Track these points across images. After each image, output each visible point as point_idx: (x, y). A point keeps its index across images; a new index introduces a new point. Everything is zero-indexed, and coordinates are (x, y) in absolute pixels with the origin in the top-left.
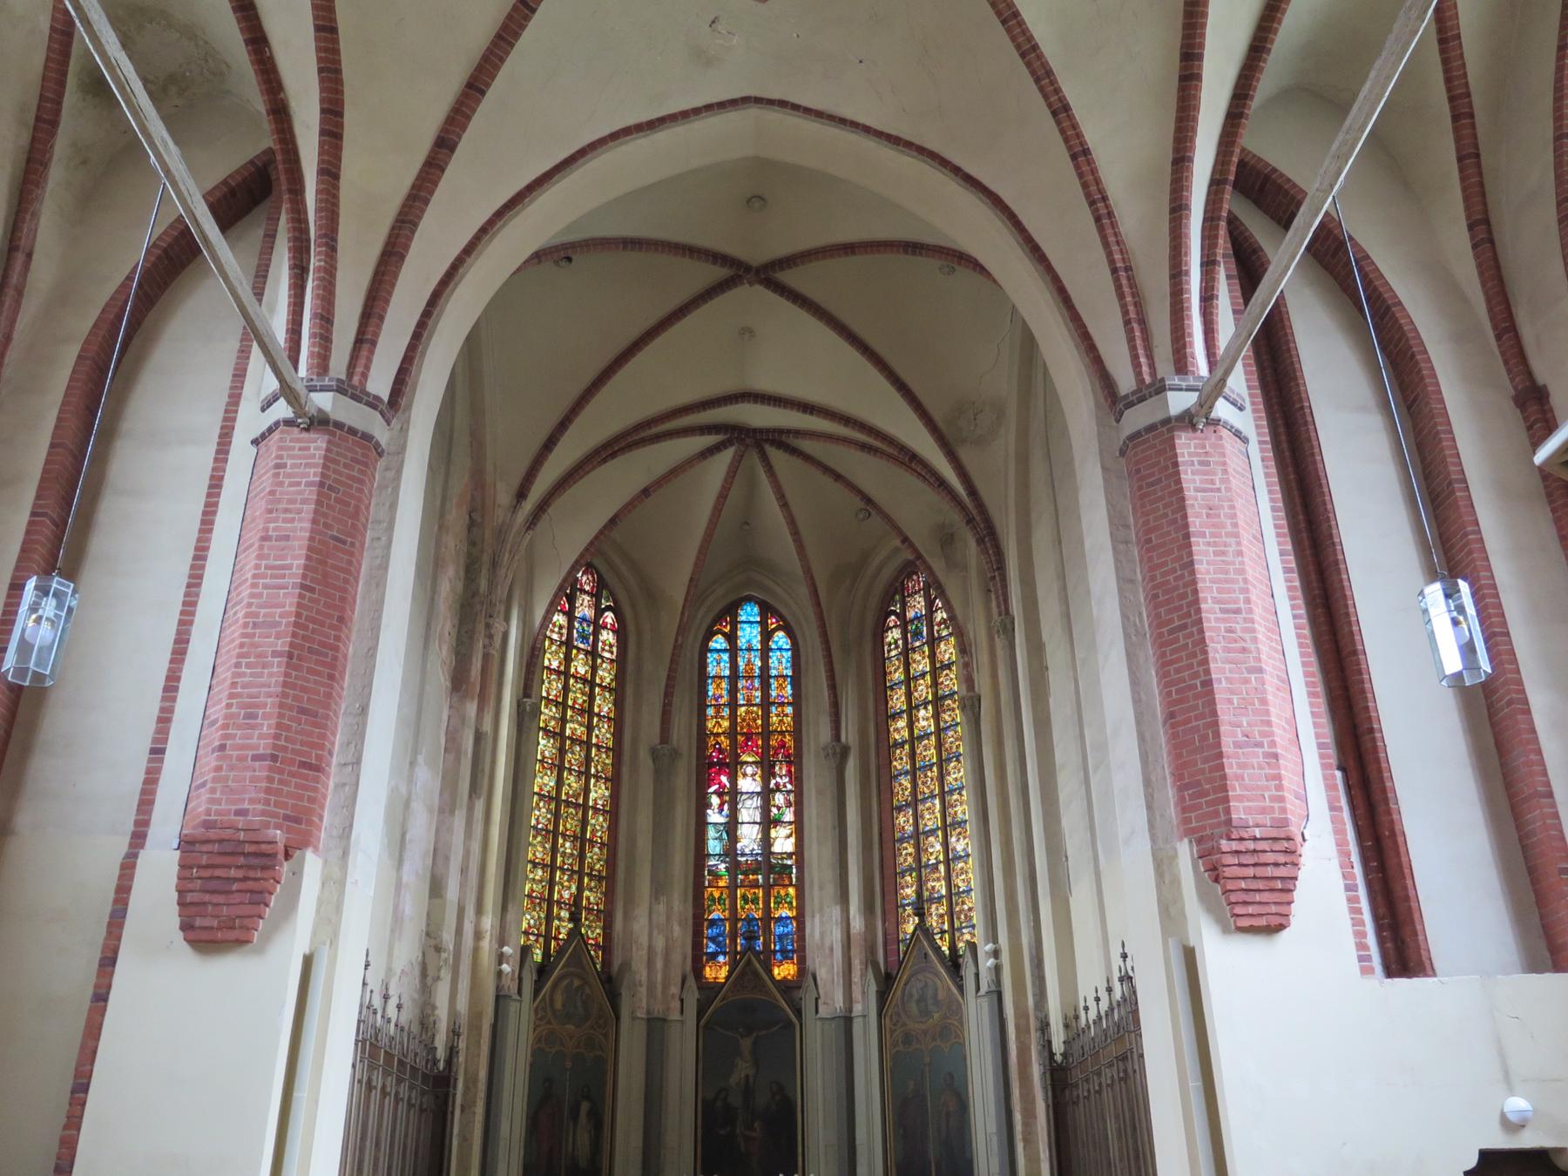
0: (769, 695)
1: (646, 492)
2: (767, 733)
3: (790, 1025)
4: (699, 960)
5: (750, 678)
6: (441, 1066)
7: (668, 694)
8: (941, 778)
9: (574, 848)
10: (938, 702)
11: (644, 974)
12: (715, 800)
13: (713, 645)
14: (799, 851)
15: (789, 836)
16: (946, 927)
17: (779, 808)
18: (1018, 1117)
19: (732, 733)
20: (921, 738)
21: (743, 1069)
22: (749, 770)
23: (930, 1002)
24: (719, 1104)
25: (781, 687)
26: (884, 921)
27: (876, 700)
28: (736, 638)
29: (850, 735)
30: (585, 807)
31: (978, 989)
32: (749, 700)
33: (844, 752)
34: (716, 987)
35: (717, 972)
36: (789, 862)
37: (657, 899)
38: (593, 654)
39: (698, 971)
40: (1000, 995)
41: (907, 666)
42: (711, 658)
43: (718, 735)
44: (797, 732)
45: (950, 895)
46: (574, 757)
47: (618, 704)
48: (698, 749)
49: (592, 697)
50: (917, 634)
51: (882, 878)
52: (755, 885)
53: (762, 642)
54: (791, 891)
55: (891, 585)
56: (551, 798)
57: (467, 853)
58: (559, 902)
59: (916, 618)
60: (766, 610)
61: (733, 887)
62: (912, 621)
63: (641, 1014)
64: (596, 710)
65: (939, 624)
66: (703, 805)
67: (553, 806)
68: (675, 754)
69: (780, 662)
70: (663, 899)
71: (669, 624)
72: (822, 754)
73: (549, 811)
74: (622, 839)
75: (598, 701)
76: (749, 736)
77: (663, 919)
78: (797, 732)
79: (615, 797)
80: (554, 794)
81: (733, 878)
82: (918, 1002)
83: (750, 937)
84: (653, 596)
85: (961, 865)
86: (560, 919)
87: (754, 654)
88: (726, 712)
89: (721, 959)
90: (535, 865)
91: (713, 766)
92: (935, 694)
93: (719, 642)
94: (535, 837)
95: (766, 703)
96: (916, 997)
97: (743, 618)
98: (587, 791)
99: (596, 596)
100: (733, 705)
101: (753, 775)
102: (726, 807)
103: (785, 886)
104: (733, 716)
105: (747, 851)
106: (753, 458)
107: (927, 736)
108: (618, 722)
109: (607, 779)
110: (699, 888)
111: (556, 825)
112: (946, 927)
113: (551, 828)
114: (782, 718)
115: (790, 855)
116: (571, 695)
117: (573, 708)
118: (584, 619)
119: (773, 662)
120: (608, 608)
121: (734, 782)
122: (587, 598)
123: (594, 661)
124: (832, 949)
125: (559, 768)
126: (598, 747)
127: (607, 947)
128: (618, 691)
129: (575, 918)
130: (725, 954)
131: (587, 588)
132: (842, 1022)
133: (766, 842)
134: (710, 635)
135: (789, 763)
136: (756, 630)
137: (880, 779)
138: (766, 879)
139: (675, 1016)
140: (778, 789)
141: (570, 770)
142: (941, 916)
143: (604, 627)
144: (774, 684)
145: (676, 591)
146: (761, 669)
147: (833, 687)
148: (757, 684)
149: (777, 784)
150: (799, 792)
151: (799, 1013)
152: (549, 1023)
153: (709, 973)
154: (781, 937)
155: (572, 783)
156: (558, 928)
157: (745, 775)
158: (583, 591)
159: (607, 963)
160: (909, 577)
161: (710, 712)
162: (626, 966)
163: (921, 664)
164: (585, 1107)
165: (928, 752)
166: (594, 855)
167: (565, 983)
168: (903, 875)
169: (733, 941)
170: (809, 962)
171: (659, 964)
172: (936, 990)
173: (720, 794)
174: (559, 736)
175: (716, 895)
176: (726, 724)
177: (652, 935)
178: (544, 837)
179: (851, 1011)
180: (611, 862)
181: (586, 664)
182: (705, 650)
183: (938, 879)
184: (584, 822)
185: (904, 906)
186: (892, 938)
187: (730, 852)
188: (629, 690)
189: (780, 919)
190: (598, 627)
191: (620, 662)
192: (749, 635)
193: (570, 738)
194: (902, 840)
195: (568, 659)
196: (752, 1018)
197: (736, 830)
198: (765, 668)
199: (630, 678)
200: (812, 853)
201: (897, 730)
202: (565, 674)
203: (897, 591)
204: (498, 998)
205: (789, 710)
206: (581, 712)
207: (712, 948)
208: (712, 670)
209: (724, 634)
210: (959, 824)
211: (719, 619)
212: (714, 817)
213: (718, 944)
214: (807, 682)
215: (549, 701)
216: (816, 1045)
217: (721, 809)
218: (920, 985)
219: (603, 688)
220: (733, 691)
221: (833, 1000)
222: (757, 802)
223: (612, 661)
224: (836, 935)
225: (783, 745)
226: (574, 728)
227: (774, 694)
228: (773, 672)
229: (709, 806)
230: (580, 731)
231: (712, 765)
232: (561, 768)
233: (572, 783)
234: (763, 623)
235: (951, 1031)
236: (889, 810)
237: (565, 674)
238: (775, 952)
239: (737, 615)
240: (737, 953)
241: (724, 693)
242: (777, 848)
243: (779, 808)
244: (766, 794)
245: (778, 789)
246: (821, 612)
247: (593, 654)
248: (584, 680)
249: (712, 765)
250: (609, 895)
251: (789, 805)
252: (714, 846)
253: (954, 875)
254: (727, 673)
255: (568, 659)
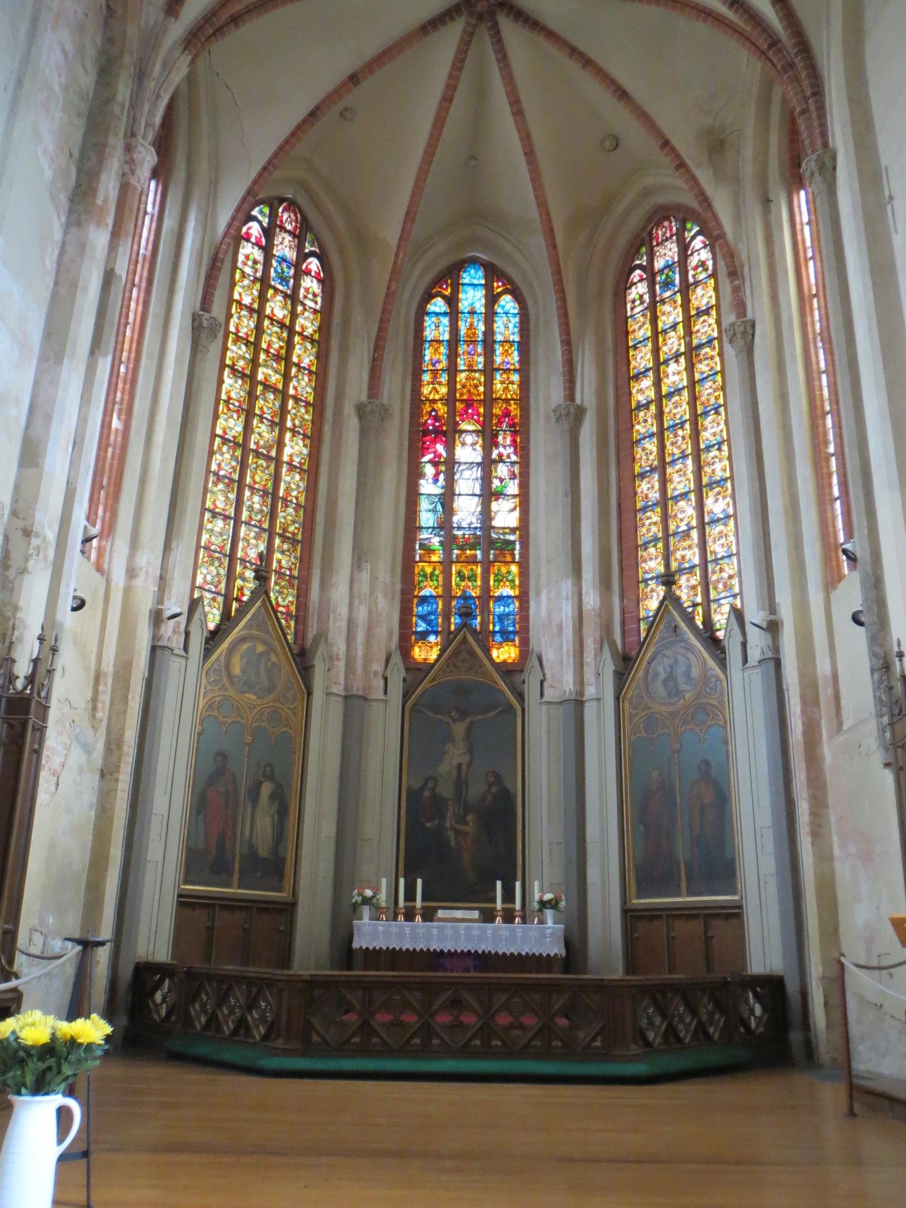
0: (493, 361)
1: (354, 79)
2: (489, 400)
3: (511, 709)
4: (407, 638)
5: (472, 342)
6: (19, 684)
7: (378, 347)
8: (696, 435)
9: (264, 503)
10: (691, 353)
11: (342, 647)
12: (429, 470)
13: (431, 308)
14: (523, 528)
15: (514, 509)
16: (699, 599)
17: (501, 480)
18: (803, 808)
19: (450, 400)
20: (670, 395)
21: (455, 755)
22: (469, 439)
23: (681, 680)
24: (427, 794)
25: (506, 353)
26: (622, 598)
27: (616, 363)
28: (458, 300)
29: (586, 394)
30: (278, 461)
31: (745, 660)
32: (470, 366)
33: (580, 413)
34: (424, 669)
35: (427, 652)
36: (512, 538)
37: (359, 566)
38: (293, 298)
39: (405, 650)
40: (778, 663)
41: (654, 320)
42: (429, 322)
43: (434, 401)
44: (524, 399)
45: (704, 562)
46: (267, 404)
47: (322, 357)
48: (412, 415)
49: (290, 345)
50: (667, 284)
51: (621, 551)
52: (473, 561)
53: (486, 306)
54: (514, 569)
55: (637, 236)
56: (236, 444)
57: (82, 421)
58: (243, 560)
59: (668, 266)
60: (492, 272)
61: (447, 563)
62: (661, 271)
63: (339, 689)
64: (295, 359)
65: (695, 268)
66: (415, 474)
67: (238, 453)
68: (385, 413)
69: (507, 326)
70: (367, 566)
71: (381, 270)
72: (553, 419)
73: (233, 457)
74: (321, 501)
75: (298, 350)
76: (469, 403)
77: (365, 589)
78: (524, 399)
79: (314, 455)
80: (240, 440)
81: (447, 550)
82: (665, 682)
83: (466, 614)
84: (363, 241)
85: (720, 527)
86: (244, 579)
87: (476, 320)
88: (444, 378)
89: (432, 638)
90: (214, 515)
91: (428, 433)
92: (689, 345)
93: (438, 305)
94: (215, 484)
95: (489, 370)
96: (663, 675)
97: (466, 281)
98: (280, 444)
99: (299, 237)
100: (452, 370)
101: (473, 444)
102: (442, 477)
103: (506, 563)
104: (452, 383)
105: (464, 524)
106: (484, 37)
107: (679, 391)
108: (320, 377)
109: (305, 436)
110: (408, 564)
111: (242, 475)
112: (699, 599)
113: (236, 477)
114: (506, 386)
115: (513, 531)
116: (265, 338)
117: (267, 352)
118: (284, 259)
119: (499, 325)
120: (312, 254)
121: (450, 448)
122: (288, 238)
123: (294, 306)
124: (560, 628)
125: (249, 414)
126: (296, 399)
127: (301, 615)
128: (322, 343)
129: (261, 577)
130: (436, 633)
131: (289, 227)
132: (572, 706)
133: (486, 515)
134: (429, 297)
135: (514, 433)
136: (480, 293)
137: (620, 445)
138: (486, 554)
139: (380, 695)
140: (501, 459)
141: (261, 418)
142: (694, 587)
143: (308, 272)
144: (499, 350)
145: (391, 234)
146: (485, 333)
147: (567, 343)
148: (480, 349)
149: (500, 455)
150: (525, 463)
151: (520, 697)
152: (224, 688)
153: (418, 653)
154: (501, 617)
155: (263, 433)
156: (241, 589)
157: (464, 444)
158: (282, 228)
159: (300, 634)
160: (659, 224)
161: (427, 377)
162: (322, 635)
163: (671, 314)
164: (267, 788)
165: (677, 409)
166: (287, 516)
167: (245, 646)
168: (645, 546)
169: (447, 616)
170: (533, 642)
171: (360, 637)
172: (689, 666)
173: (435, 463)
174: (249, 377)
175: (429, 570)
176: (444, 390)
177: (355, 608)
178: (228, 485)
179: (582, 694)
180: (308, 525)
181: (284, 307)
182: (422, 313)
183: (690, 547)
184: (277, 478)
185: (645, 581)
186: (630, 616)
187: (445, 525)
188: (335, 344)
189: (500, 598)
190: (300, 273)
191: (325, 313)
192: (472, 298)
193: (261, 383)
194: (644, 509)
195: (262, 298)
196: (464, 699)
197: (452, 501)
198: (489, 332)
199: (336, 330)
200: (537, 528)
201: (641, 391)
202: (258, 312)
203: (644, 241)
204: (154, 649)
205: (515, 377)
206: (277, 358)
207: (422, 627)
208: (429, 333)
209: (444, 297)
210: (718, 483)
211: (439, 280)
212: (429, 487)
213: (429, 623)
214: (538, 348)
215: (238, 339)
216: (541, 731)
217: (436, 480)
218: (668, 662)
219: (304, 338)
220: (453, 355)
221: (562, 681)
222: (477, 473)
223: (315, 311)
224: (567, 611)
225: (507, 413)
226: (268, 373)
227: (498, 360)
228: (499, 338)
229: (422, 475)
230: (275, 378)
231: (426, 433)
232: (249, 415)
233: (263, 433)
234: (488, 287)
235: (708, 709)
236: (628, 480)
237: (258, 312)
238: (494, 633)
239: (459, 277)
240: (450, 633)
241: (443, 358)
242: (496, 523)
243: (501, 480)
244: (487, 465)
245: (501, 459)
246: (557, 255)
247: (293, 298)
248: (282, 325)
249: (426, 433)
250: (305, 561)
251: (513, 476)
252: (427, 518)
253: (710, 540)
254: (446, 337)
255: (262, 298)
